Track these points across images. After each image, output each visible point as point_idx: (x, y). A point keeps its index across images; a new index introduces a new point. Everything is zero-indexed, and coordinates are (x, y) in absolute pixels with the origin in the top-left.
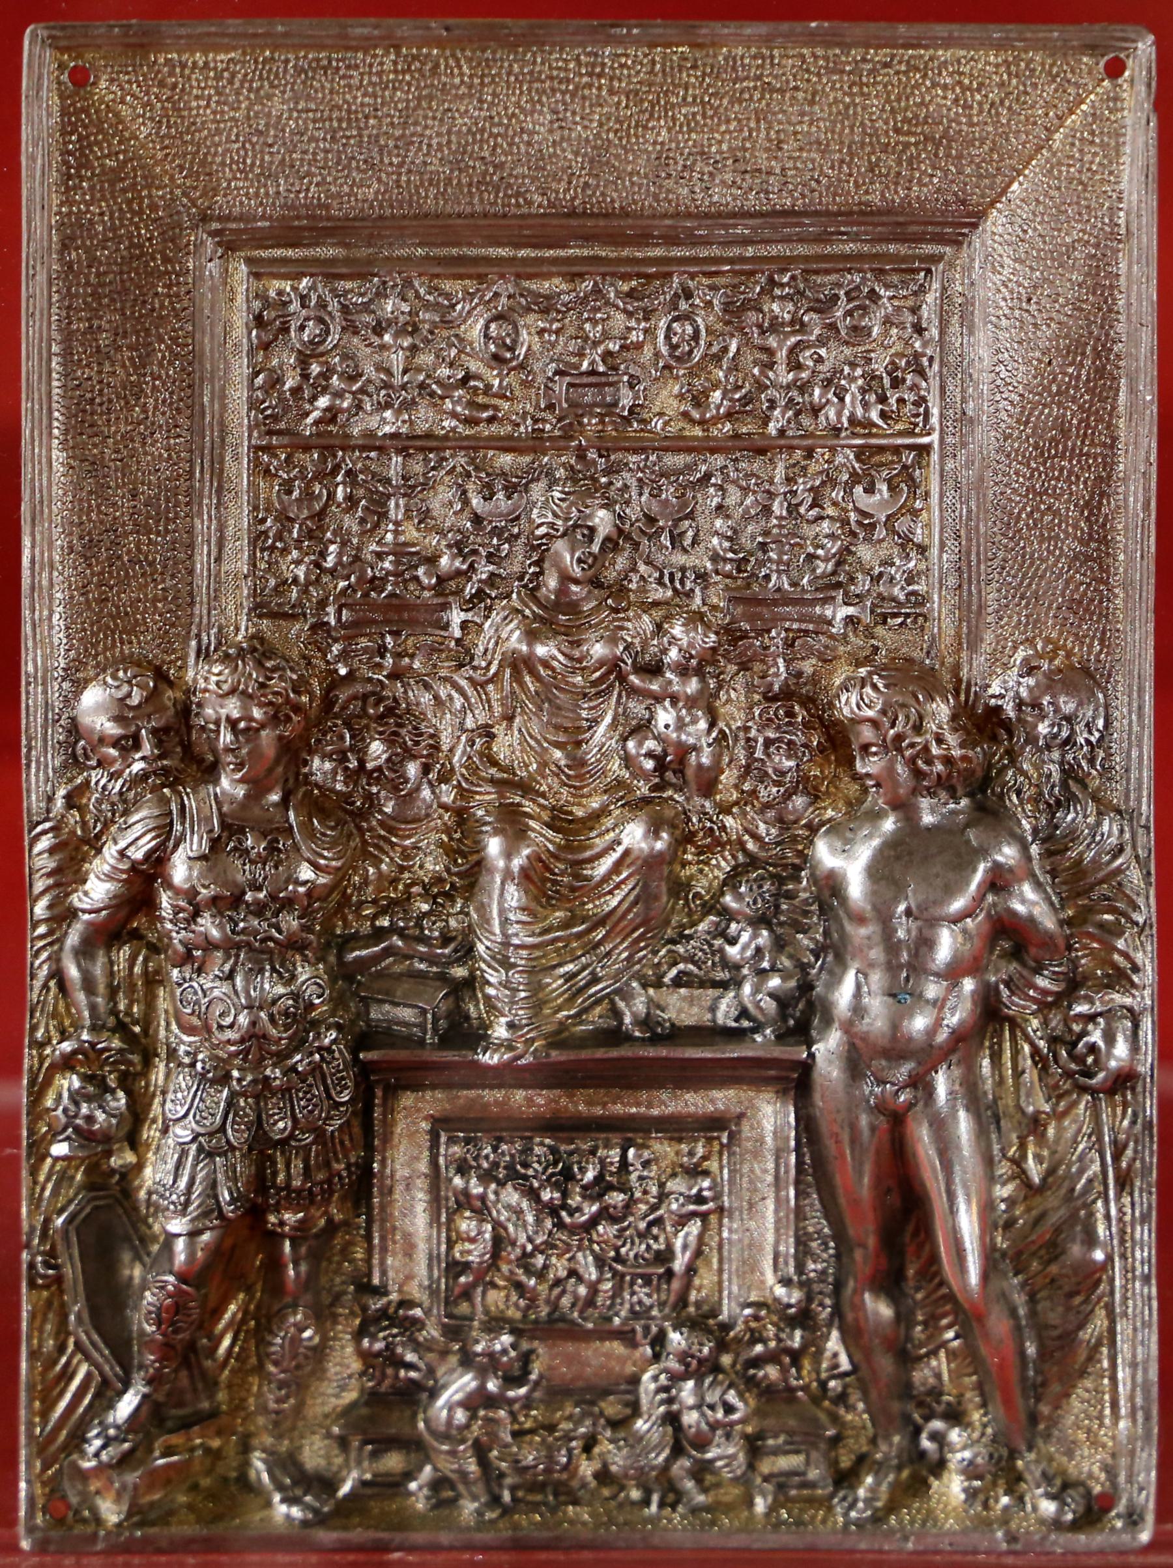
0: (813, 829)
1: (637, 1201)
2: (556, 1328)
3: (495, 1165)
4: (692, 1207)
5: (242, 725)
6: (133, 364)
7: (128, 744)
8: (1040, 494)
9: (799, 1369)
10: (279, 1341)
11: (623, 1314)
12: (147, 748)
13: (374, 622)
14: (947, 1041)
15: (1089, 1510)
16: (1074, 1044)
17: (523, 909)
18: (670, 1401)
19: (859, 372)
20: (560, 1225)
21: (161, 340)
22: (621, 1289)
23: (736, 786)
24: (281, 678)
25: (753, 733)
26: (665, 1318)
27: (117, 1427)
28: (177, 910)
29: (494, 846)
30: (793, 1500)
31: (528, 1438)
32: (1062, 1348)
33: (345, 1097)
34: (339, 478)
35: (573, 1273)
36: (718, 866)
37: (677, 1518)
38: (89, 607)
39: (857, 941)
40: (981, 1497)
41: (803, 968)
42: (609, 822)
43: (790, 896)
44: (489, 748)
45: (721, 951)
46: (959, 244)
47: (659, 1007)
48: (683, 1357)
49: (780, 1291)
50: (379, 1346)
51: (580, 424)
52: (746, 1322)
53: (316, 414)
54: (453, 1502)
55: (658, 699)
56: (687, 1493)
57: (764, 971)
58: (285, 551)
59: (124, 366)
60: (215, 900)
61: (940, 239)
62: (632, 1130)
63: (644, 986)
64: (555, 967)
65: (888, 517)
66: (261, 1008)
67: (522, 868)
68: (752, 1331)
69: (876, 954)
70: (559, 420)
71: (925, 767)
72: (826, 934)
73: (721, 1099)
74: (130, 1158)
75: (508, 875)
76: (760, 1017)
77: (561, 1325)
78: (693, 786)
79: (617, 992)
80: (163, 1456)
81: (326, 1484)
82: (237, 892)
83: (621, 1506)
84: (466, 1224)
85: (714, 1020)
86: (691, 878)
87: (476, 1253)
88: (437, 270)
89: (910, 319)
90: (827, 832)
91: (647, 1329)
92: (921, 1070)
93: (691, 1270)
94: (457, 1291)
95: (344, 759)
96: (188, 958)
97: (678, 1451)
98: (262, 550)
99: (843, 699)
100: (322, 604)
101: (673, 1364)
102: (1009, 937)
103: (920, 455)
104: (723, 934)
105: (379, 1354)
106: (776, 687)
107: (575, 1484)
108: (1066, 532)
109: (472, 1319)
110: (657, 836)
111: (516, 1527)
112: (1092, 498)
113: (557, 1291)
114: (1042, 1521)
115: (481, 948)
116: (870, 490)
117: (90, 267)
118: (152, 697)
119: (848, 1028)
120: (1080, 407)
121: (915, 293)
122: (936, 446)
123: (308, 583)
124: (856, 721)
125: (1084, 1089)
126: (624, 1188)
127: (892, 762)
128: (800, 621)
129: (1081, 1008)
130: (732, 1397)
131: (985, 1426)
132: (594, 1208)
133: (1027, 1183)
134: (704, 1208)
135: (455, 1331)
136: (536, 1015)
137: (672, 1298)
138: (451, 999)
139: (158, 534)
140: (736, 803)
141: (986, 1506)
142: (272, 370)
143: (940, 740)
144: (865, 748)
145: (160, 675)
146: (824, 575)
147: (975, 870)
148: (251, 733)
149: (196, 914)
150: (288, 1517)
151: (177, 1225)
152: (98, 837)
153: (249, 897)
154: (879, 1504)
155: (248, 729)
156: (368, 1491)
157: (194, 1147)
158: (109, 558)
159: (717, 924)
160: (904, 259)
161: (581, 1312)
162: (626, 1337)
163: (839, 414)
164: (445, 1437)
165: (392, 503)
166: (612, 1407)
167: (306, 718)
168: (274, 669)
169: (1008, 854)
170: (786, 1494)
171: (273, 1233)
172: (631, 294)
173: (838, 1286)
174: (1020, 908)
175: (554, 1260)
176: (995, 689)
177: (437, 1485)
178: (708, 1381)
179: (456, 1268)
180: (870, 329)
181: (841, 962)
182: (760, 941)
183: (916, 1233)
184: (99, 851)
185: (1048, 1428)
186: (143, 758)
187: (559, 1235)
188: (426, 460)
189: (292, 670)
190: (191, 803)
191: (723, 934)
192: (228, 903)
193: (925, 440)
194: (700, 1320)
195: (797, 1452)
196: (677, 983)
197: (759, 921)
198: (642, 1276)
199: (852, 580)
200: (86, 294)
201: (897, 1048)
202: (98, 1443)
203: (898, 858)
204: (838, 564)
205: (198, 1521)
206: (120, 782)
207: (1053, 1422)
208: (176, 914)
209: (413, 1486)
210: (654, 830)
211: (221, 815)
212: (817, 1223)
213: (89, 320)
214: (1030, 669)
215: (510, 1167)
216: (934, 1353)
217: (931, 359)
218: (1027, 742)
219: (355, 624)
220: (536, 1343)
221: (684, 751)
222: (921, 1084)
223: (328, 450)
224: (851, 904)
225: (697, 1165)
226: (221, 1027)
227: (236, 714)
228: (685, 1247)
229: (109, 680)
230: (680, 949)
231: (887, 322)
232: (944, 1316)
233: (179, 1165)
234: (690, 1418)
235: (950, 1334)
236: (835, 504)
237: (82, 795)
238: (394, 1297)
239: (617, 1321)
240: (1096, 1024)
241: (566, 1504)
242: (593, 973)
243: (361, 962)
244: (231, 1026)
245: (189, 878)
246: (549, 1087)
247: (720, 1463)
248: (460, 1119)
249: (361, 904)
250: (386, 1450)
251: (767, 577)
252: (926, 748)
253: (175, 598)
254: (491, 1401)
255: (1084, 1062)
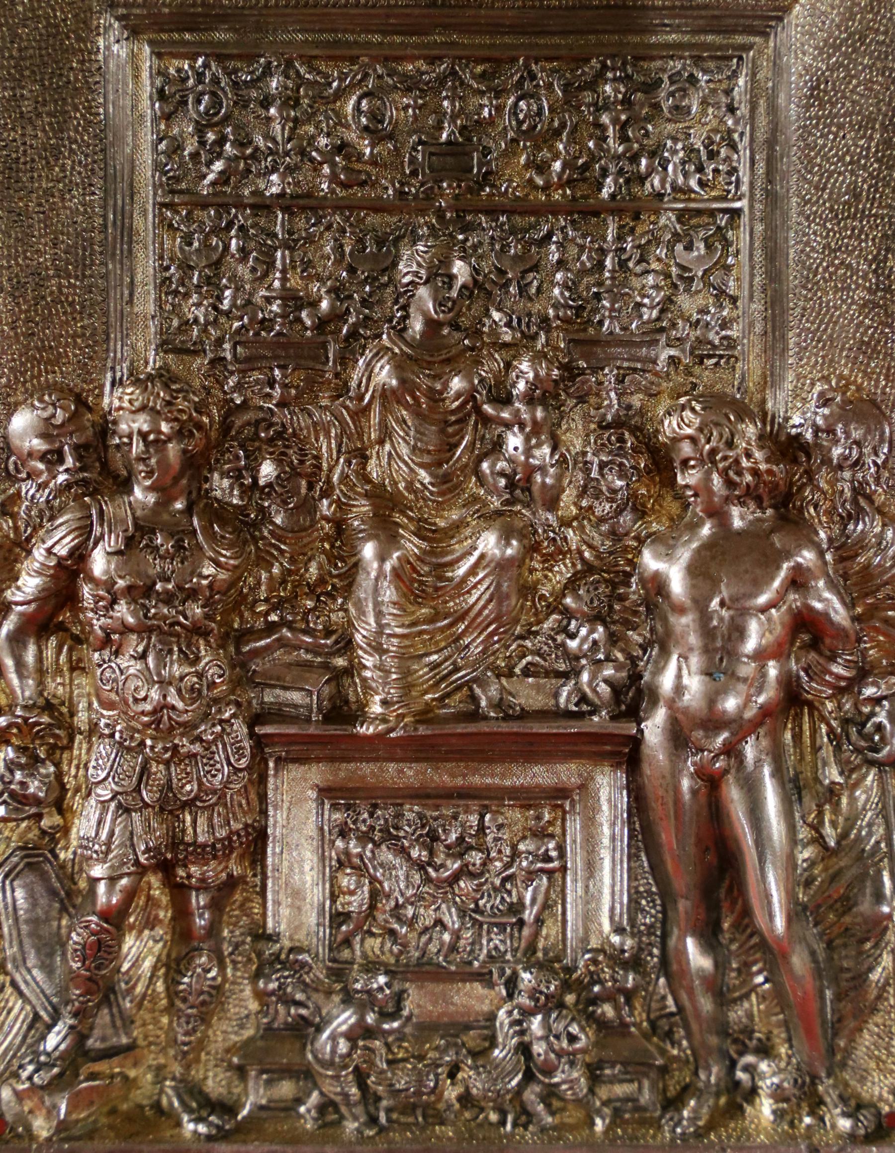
0: (641, 541)
1: (492, 860)
2: (426, 971)
3: (372, 828)
4: (539, 865)
5: (152, 437)
6: (52, 129)
7: (53, 458)
8: (835, 251)
9: (632, 1008)
10: (186, 980)
11: (481, 958)
12: (69, 462)
13: (265, 357)
14: (755, 716)
15: (879, 1126)
16: (864, 725)
17: (395, 603)
18: (522, 1033)
19: (680, 146)
20: (428, 880)
21: (77, 109)
22: (480, 935)
23: (575, 504)
24: (185, 399)
25: (589, 457)
26: (517, 962)
27: (48, 1054)
28: (98, 599)
29: (368, 550)
30: (627, 1122)
31: (401, 1065)
32: (855, 987)
33: (243, 763)
34: (233, 233)
35: (439, 922)
36: (560, 573)
37: (528, 1136)
38: (18, 341)
39: (678, 629)
40: (788, 1118)
41: (633, 660)
42: (468, 532)
43: (622, 598)
44: (364, 469)
45: (563, 645)
46: (766, 35)
47: (510, 694)
48: (534, 994)
49: (616, 939)
50: (273, 986)
51: (440, 188)
52: (587, 966)
53: (211, 177)
54: (338, 1123)
55: (508, 426)
56: (537, 1115)
57: (600, 661)
58: (187, 296)
59: (44, 130)
60: (130, 589)
61: (751, 31)
62: (488, 798)
63: (498, 676)
64: (422, 656)
65: (705, 272)
66: (170, 683)
67: (394, 569)
68: (591, 973)
69: (693, 639)
70: (422, 185)
71: (737, 479)
72: (652, 630)
73: (566, 773)
74: (57, 820)
75: (381, 574)
76: (596, 701)
77: (428, 968)
78: (540, 503)
79: (475, 680)
80: (87, 1079)
81: (227, 1109)
82: (149, 582)
83: (480, 1125)
84: (347, 881)
85: (557, 704)
86: (538, 581)
87: (356, 902)
88: (316, 52)
89: (724, 100)
90: (653, 542)
91: (502, 972)
92: (734, 740)
93: (539, 921)
94: (340, 938)
95: (239, 477)
96: (107, 641)
97: (529, 1077)
98: (167, 294)
99: (666, 423)
100: (219, 342)
101: (524, 1000)
102: (807, 629)
103: (732, 218)
104: (564, 630)
105: (273, 993)
106: (609, 417)
107: (441, 1106)
108: (856, 283)
109: (352, 963)
110: (508, 544)
111: (390, 1142)
112: (879, 253)
113: (424, 939)
114: (840, 1136)
115: (358, 638)
116: (689, 248)
117: (12, 42)
118: (74, 417)
119: (671, 705)
120: (870, 174)
121: (729, 78)
122: (746, 210)
123: (207, 323)
124: (677, 440)
125: (871, 763)
126: (481, 848)
127: (708, 474)
128: (628, 360)
129: (870, 691)
130: (574, 1029)
131: (789, 1057)
132: (456, 866)
133: (825, 847)
134: (551, 865)
135: (339, 972)
136: (406, 695)
137: (523, 944)
138: (333, 683)
139: (77, 278)
140: (576, 518)
141: (792, 1124)
142: (174, 138)
143: (749, 455)
144: (685, 463)
145: (80, 401)
146: (649, 321)
147: (779, 568)
148: (160, 444)
149: (114, 602)
150: (195, 1132)
151: (98, 871)
152: (28, 540)
153: (158, 587)
154: (701, 1123)
155: (156, 441)
156: (264, 1114)
157: (113, 805)
158: (34, 298)
159: (560, 622)
160: (720, 48)
161: (446, 956)
162: (484, 978)
163: (663, 182)
164: (330, 1064)
165: (279, 254)
166: (471, 1039)
167: (207, 437)
168: (178, 391)
169: (807, 557)
170: (622, 1118)
171: (182, 885)
172: (483, 76)
173: (665, 937)
174: (818, 606)
175: (422, 911)
176: (796, 420)
177: (323, 1108)
178: (554, 1016)
179: (339, 918)
180: (689, 108)
181: (665, 653)
182: (596, 636)
183: (730, 890)
184: (29, 552)
185: (844, 1058)
186: (67, 470)
187: (426, 889)
188: (308, 220)
189: (194, 393)
190: (109, 509)
191: (564, 630)
192: (140, 593)
193: (737, 205)
194: (549, 964)
195: (631, 1081)
196: (526, 673)
197: (596, 618)
198: (496, 925)
199: (674, 325)
200: (10, 67)
201: (713, 722)
202: (31, 1068)
203: (713, 558)
204: (662, 311)
205: (117, 1136)
206: (47, 491)
207: (848, 1052)
208: (96, 603)
209: (302, 1109)
210: (506, 536)
211: (135, 518)
212: (647, 882)
213: (13, 89)
214: (825, 401)
215: (385, 830)
216: (747, 996)
217: (742, 134)
218: (823, 463)
219: (248, 360)
220: (407, 985)
221: (530, 470)
222: (732, 750)
223: (222, 207)
224: (673, 596)
225: (544, 829)
226: (136, 700)
227: (145, 428)
228: (534, 901)
229: (36, 403)
230: (528, 643)
231: (704, 103)
232: (755, 962)
233: (100, 822)
234: (539, 1048)
235: (760, 979)
236: (659, 260)
237: (14, 504)
238: (287, 944)
239: (476, 964)
240: (882, 706)
241: (434, 1124)
242: (454, 663)
243: (256, 653)
244: (145, 699)
245: (107, 572)
246: (417, 760)
247: (564, 1087)
248: (341, 789)
249: (256, 601)
250: (281, 1079)
251: (601, 323)
252: (737, 462)
253: (93, 335)
254: (369, 1033)
255: (872, 740)
